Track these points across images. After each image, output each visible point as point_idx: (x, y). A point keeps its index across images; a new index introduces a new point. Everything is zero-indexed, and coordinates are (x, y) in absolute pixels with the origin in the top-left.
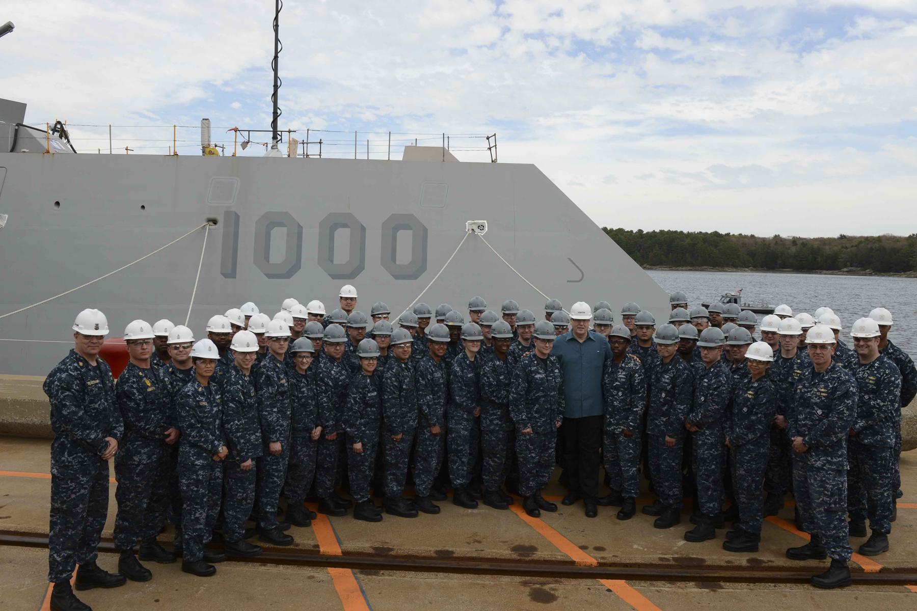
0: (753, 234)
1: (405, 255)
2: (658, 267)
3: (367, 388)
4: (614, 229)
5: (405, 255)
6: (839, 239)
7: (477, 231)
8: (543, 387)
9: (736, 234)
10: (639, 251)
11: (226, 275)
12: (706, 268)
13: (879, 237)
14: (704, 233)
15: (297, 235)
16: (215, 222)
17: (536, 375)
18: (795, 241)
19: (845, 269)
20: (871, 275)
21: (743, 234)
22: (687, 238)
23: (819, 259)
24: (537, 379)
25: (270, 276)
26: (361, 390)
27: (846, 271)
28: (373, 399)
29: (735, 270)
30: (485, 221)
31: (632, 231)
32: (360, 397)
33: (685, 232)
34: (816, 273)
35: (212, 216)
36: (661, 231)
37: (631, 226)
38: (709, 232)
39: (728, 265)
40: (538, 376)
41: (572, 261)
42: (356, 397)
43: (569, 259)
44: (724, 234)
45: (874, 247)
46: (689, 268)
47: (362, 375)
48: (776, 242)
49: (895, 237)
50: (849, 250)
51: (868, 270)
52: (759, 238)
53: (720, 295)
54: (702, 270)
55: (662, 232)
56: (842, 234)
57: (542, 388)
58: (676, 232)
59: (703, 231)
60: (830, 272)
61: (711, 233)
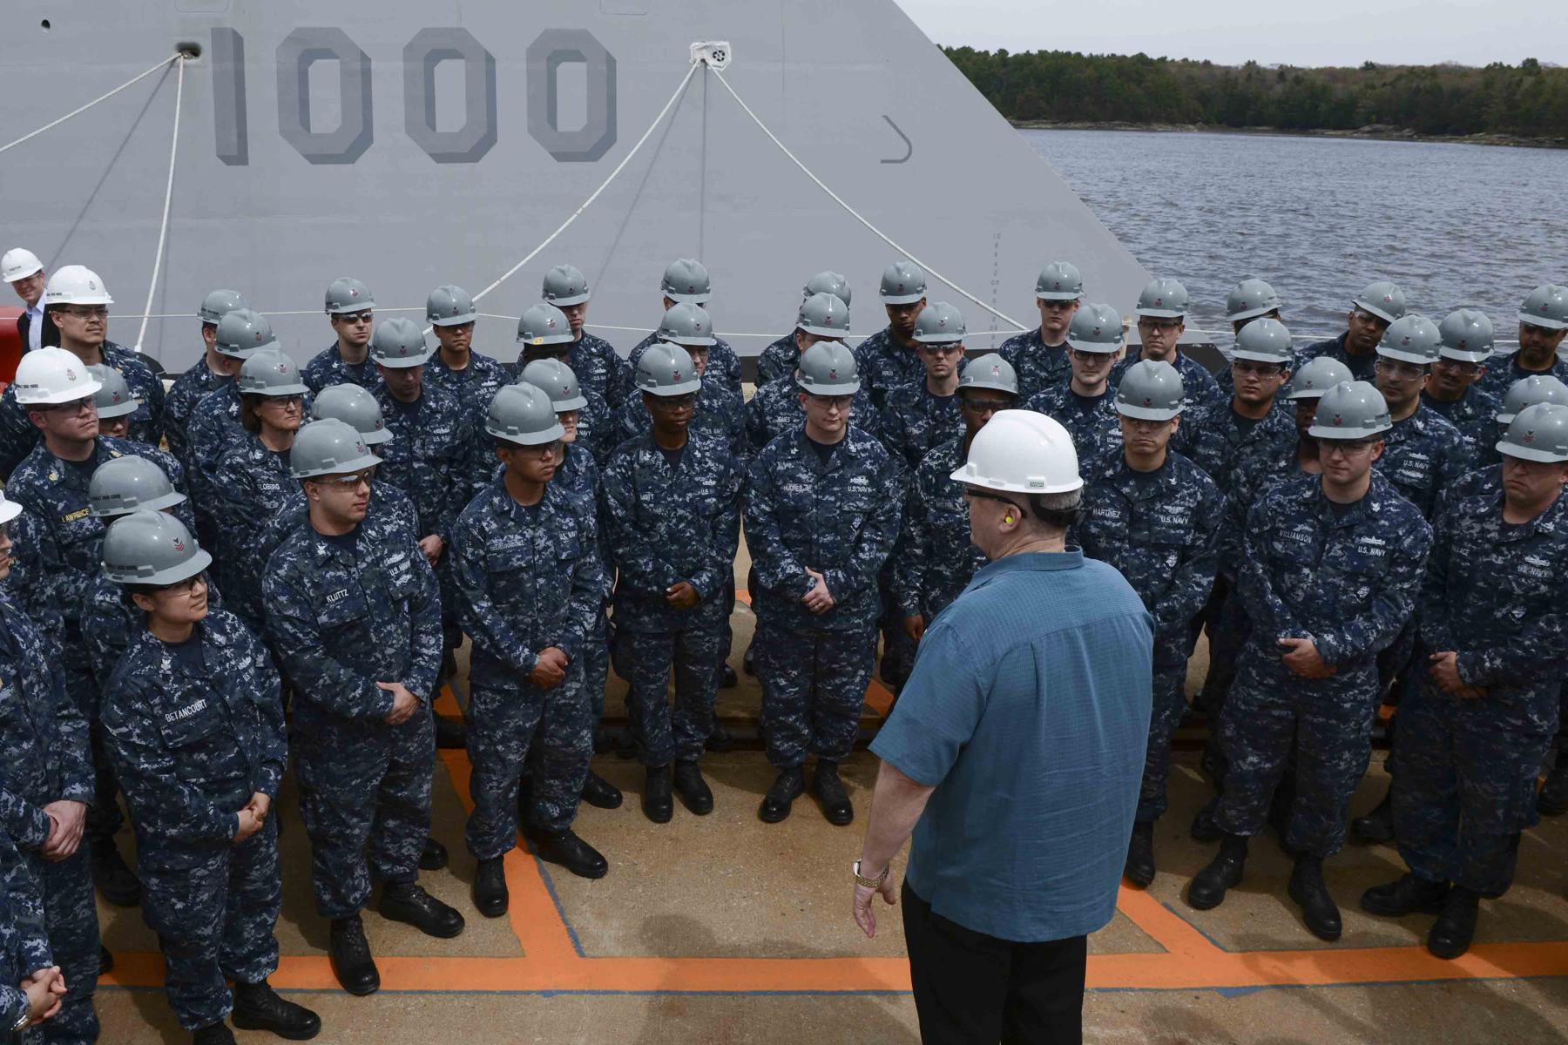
0: (1208, 59)
1: (573, 115)
2: (1032, 122)
3: (160, 692)
4: (955, 49)
5: (573, 115)
6: (1362, 69)
7: (712, 62)
8: (801, 519)
9: (1178, 58)
10: (999, 91)
11: (228, 160)
12: (1120, 125)
13: (1434, 67)
14: (1119, 57)
15: (362, 76)
16: (193, 50)
17: (785, 483)
18: (1283, 73)
19: (1367, 128)
20: (1410, 138)
21: (1190, 59)
22: (1087, 66)
23: (1323, 107)
24: (786, 495)
25: (315, 159)
26: (139, 705)
27: (1369, 132)
28: (188, 731)
29: (1170, 128)
30: (726, 43)
31: (987, 53)
32: (144, 728)
33: (1085, 54)
34: (1314, 135)
35: (188, 39)
36: (1040, 52)
37: (986, 42)
38: (1129, 55)
39: (1158, 120)
40: (791, 488)
41: (889, 121)
42: (129, 734)
43: (886, 117)
44: (1155, 58)
45: (1421, 86)
46: (1089, 124)
47: (144, 644)
48: (1249, 75)
49: (1461, 68)
50: (1377, 91)
51: (1407, 130)
52: (1219, 67)
53: (1330, 305)
54: (1112, 129)
55: (1042, 54)
56: (1369, 60)
57: (796, 521)
58: (1068, 54)
59: (1119, 53)
60: (1339, 132)
61: (1133, 57)
